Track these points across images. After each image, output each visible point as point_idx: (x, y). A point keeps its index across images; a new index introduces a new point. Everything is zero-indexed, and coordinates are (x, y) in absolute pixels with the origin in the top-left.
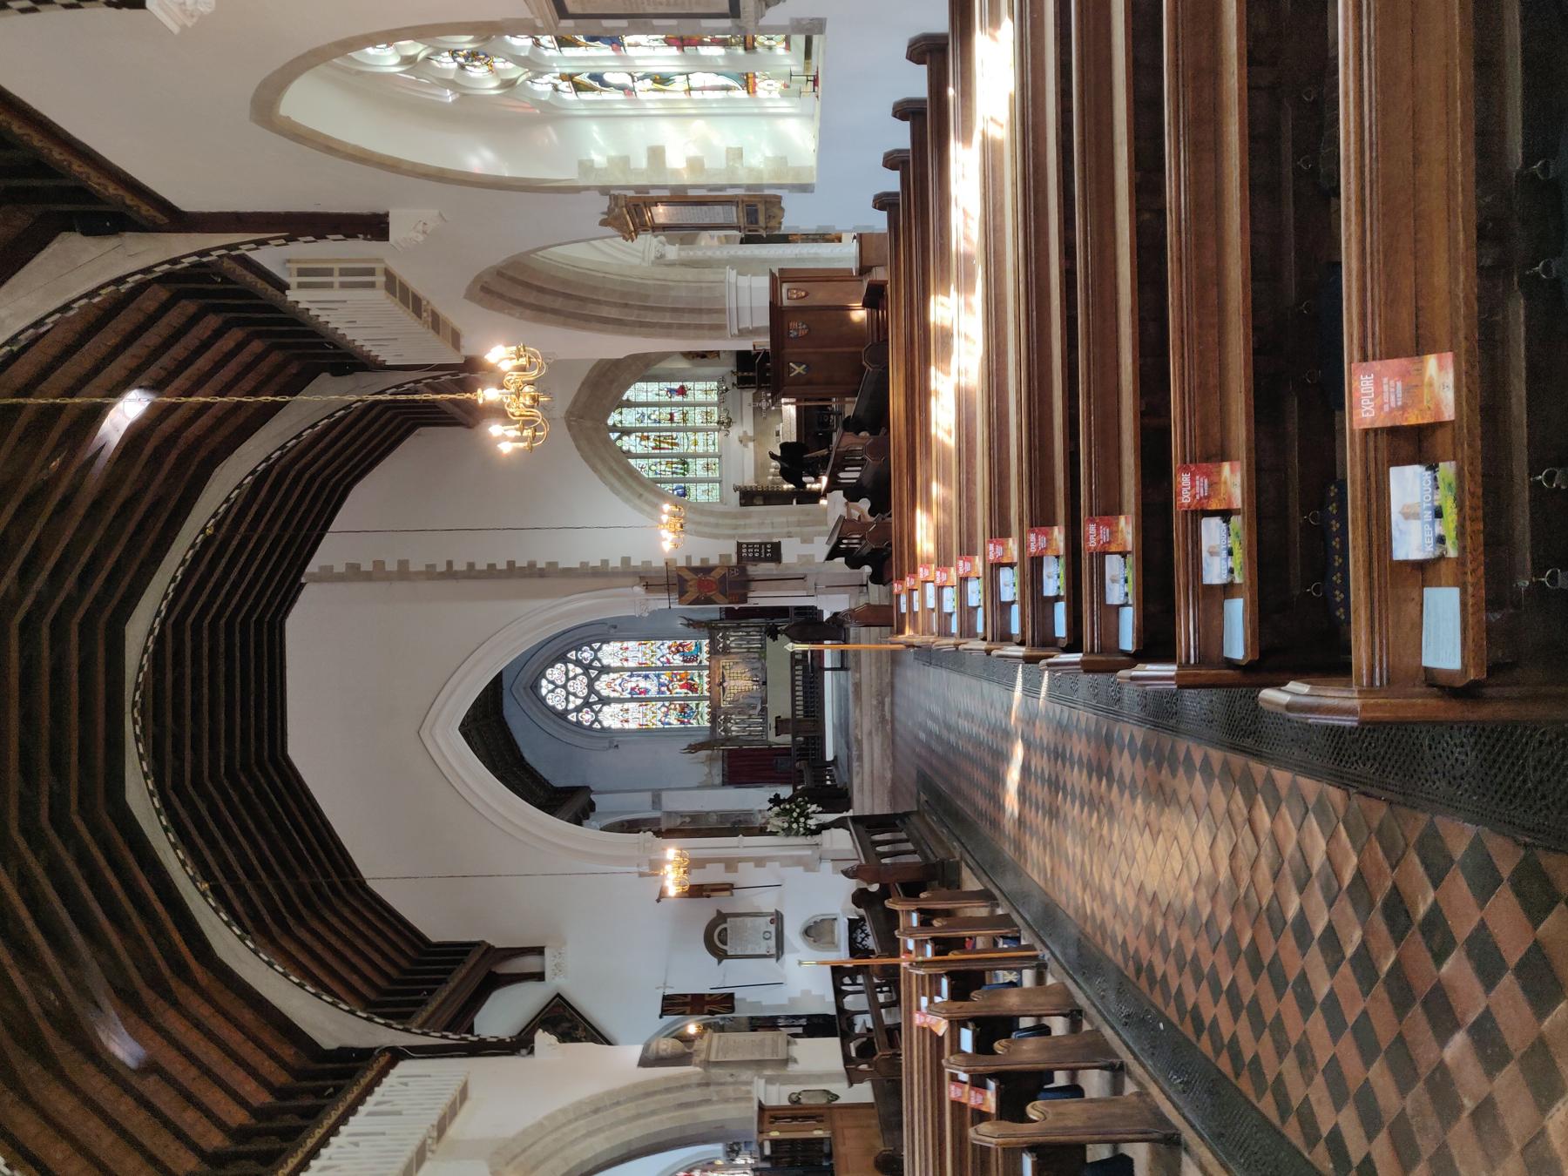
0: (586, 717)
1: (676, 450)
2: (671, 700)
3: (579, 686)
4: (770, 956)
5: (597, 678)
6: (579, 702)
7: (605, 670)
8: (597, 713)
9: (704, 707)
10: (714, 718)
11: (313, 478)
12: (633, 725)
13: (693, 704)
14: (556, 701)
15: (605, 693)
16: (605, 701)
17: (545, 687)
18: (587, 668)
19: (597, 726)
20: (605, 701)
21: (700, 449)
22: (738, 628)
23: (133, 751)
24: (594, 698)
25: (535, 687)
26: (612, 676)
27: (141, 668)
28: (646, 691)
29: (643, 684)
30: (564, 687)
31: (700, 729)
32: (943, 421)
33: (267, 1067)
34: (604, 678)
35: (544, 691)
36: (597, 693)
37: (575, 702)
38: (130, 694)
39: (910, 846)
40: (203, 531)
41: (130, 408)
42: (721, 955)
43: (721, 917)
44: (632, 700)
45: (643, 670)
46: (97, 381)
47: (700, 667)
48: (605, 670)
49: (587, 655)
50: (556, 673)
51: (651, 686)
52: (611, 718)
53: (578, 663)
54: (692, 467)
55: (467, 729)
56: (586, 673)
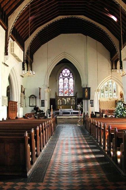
0: (61, 76)
1: (105, 91)
2: (64, 90)
3: (66, 75)
4: (30, 104)
5: (67, 78)
6: (64, 75)
7: (69, 79)
8: (62, 78)
9: (62, 95)
10: (60, 97)
11: (103, 38)
12: (60, 84)
13: (63, 93)
14: (64, 71)
15: (65, 79)
16: (64, 79)
17: (66, 70)
18: (69, 76)
19: (60, 78)
20: (64, 79)
21: (105, 95)
22: (76, 101)
23: (66, 17)
24: (64, 77)
25: (66, 68)
26: (68, 80)
27: (77, 17)
28: (65, 86)
29: (66, 85)
30: (66, 73)
31: (59, 94)
32: (85, 156)
33: (23, 36)
34: (67, 79)
35: (65, 69)
36: (65, 78)
37: (63, 74)
38: (74, 16)
39: (33, 131)
40: (96, 25)
41: (115, 19)
42: (30, 97)
43: (36, 97)
44: (64, 83)
45: (69, 85)
46: (123, 25)
47: (69, 95)
48: (69, 79)
49: (71, 76)
50: (68, 71)
51: (66, 87)
52: (61, 80)
53: (70, 75)
54: (103, 93)
55: (64, 59)
56: (68, 76)
